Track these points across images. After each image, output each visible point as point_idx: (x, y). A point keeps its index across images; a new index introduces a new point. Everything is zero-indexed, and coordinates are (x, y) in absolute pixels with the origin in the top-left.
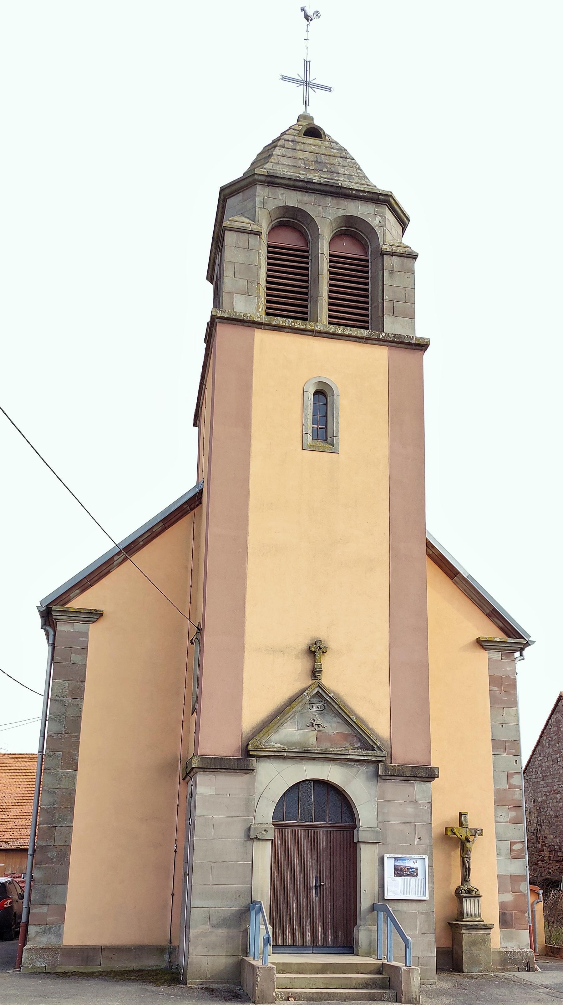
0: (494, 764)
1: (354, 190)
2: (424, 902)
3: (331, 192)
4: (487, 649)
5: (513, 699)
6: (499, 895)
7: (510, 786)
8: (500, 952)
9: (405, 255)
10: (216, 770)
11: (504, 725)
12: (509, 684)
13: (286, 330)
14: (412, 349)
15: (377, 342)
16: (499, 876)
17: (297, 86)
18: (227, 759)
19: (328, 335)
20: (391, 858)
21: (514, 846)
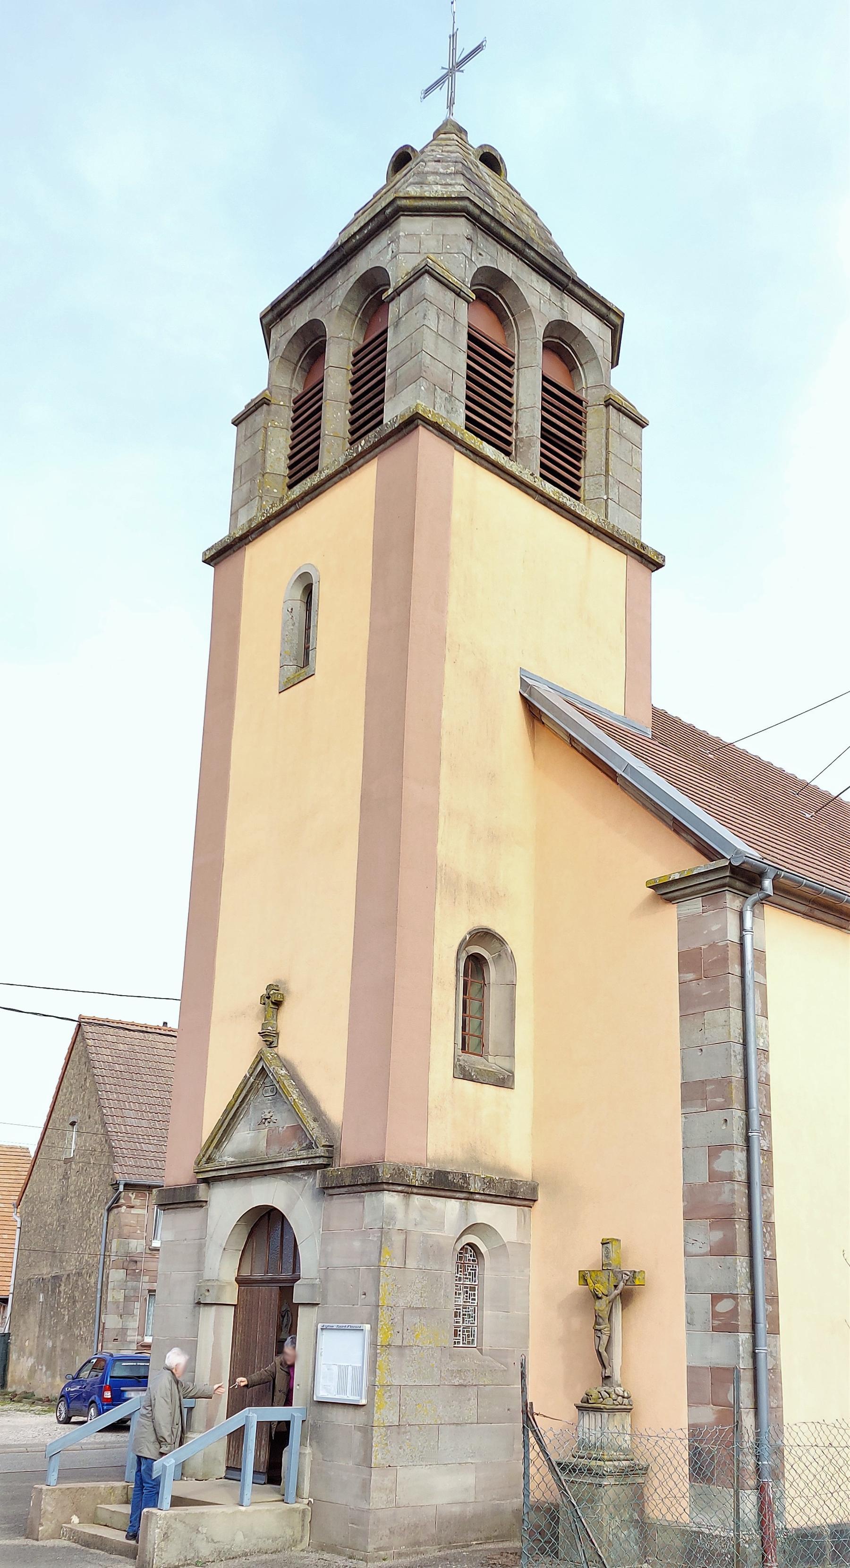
0: (684, 1133)
1: (355, 234)
2: (362, 1409)
3: (337, 264)
4: (673, 900)
5: (721, 990)
6: (690, 1409)
7: (714, 1176)
8: (683, 1532)
9: (411, 279)
10: (498, 1199)
11: (704, 1048)
12: (715, 960)
13: (271, 524)
14: (405, 436)
15: (362, 461)
16: (691, 1370)
17: (441, 89)
18: (178, 1188)
19: (310, 495)
20: (336, 1331)
21: (719, 1304)
